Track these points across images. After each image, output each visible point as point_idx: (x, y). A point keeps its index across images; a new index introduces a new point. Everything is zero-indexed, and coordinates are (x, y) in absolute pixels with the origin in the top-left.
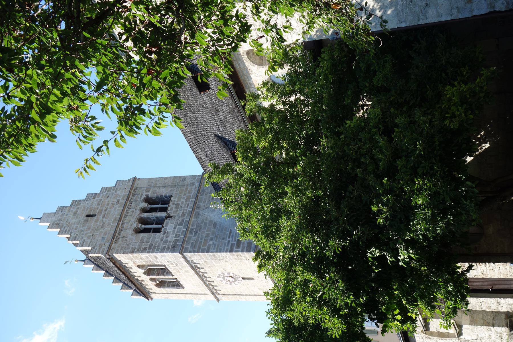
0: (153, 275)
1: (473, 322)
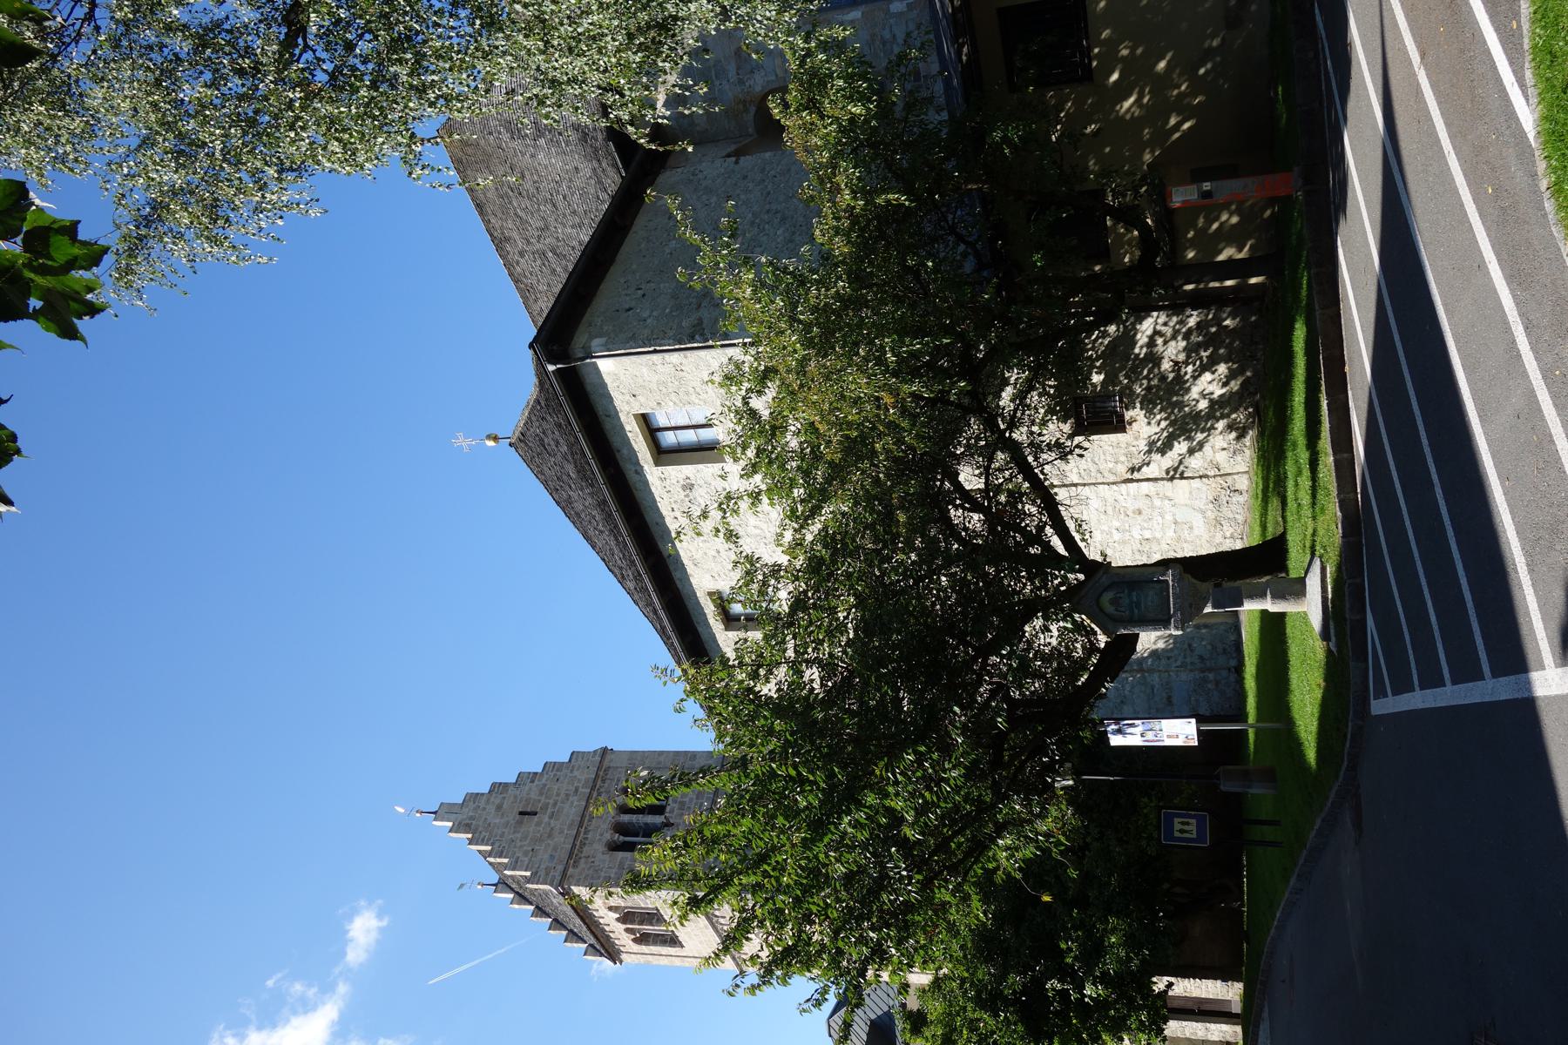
0: (632, 922)
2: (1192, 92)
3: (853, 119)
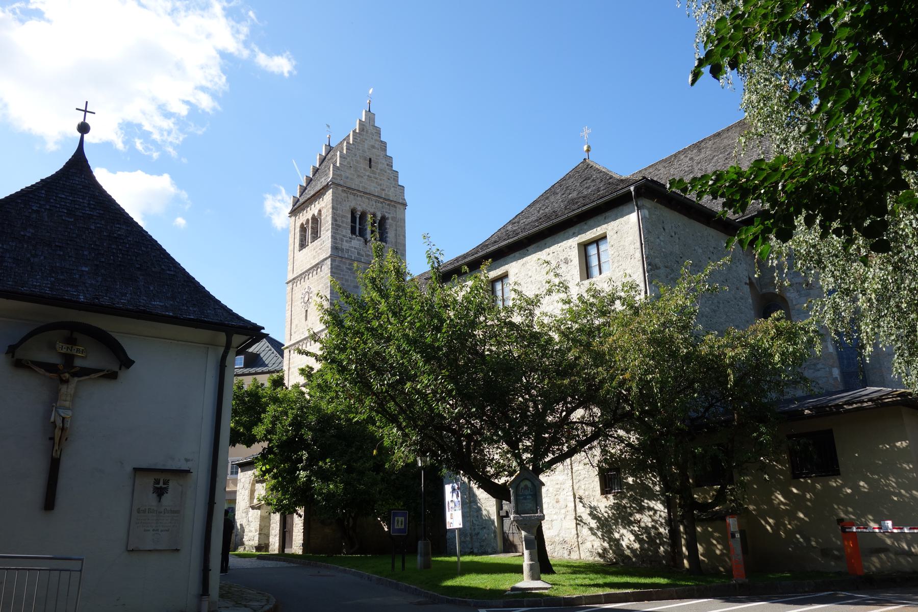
1: (263, 519)
2: (787, 531)
3: (771, 356)
